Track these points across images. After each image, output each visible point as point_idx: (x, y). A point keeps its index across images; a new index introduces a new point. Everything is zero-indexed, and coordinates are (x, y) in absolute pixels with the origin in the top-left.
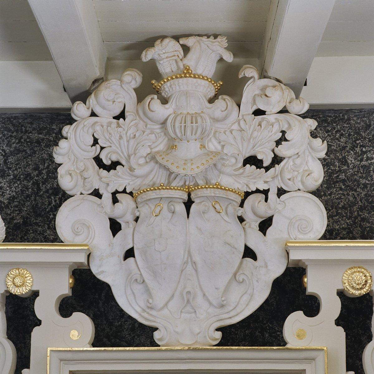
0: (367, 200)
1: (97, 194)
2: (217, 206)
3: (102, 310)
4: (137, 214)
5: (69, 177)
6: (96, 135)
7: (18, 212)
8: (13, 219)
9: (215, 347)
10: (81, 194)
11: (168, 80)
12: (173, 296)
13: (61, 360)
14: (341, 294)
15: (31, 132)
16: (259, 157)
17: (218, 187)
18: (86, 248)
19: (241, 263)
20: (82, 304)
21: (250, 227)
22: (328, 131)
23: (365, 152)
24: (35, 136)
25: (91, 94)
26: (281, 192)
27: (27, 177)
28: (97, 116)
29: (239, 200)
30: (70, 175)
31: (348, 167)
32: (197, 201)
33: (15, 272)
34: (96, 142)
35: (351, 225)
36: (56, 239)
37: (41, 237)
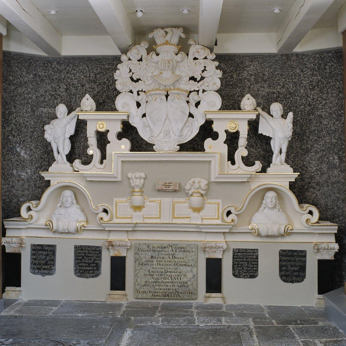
0: (241, 93)
1: (131, 92)
2: (178, 97)
3: (134, 137)
4: (147, 100)
5: (120, 85)
6: (130, 68)
7: (101, 98)
8: (99, 100)
9: (177, 152)
10: (125, 92)
11: (159, 46)
12: (161, 132)
13: (118, 157)
14: (226, 131)
15: (105, 65)
16: (195, 77)
17: (179, 89)
18: (127, 114)
19: (188, 119)
20: (127, 134)
21: (191, 105)
22: (226, 64)
23: (241, 73)
24: (107, 66)
25: (129, 50)
26: (204, 91)
27: (104, 83)
28: (131, 60)
29: (187, 94)
30: (121, 84)
31: (234, 79)
32: (170, 95)
33: (100, 123)
34: (130, 71)
35: (234, 103)
36: (115, 110)
37: (110, 108)
